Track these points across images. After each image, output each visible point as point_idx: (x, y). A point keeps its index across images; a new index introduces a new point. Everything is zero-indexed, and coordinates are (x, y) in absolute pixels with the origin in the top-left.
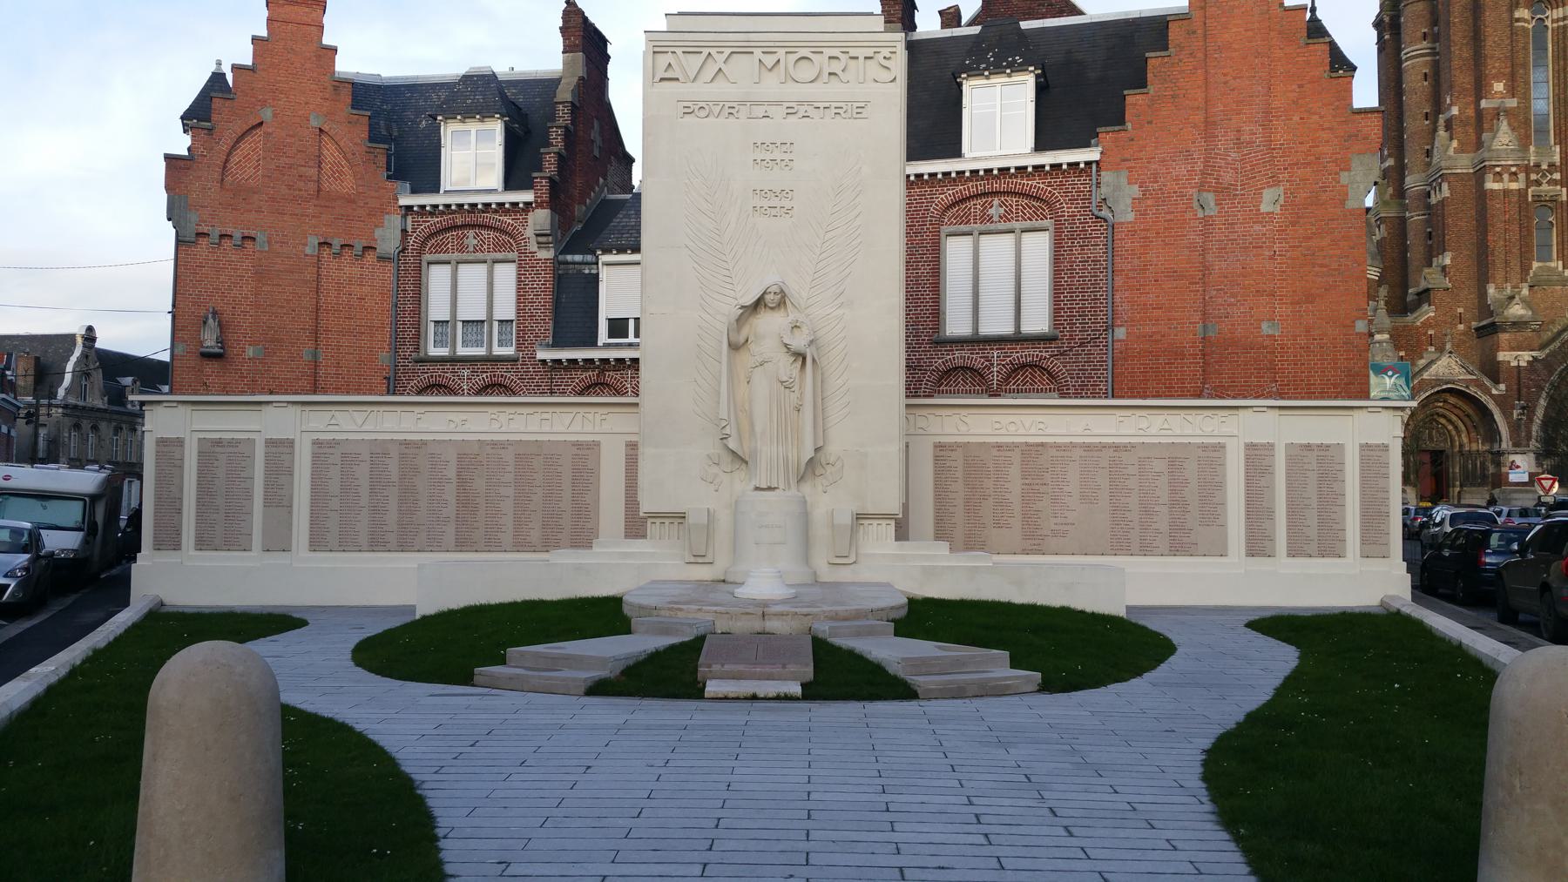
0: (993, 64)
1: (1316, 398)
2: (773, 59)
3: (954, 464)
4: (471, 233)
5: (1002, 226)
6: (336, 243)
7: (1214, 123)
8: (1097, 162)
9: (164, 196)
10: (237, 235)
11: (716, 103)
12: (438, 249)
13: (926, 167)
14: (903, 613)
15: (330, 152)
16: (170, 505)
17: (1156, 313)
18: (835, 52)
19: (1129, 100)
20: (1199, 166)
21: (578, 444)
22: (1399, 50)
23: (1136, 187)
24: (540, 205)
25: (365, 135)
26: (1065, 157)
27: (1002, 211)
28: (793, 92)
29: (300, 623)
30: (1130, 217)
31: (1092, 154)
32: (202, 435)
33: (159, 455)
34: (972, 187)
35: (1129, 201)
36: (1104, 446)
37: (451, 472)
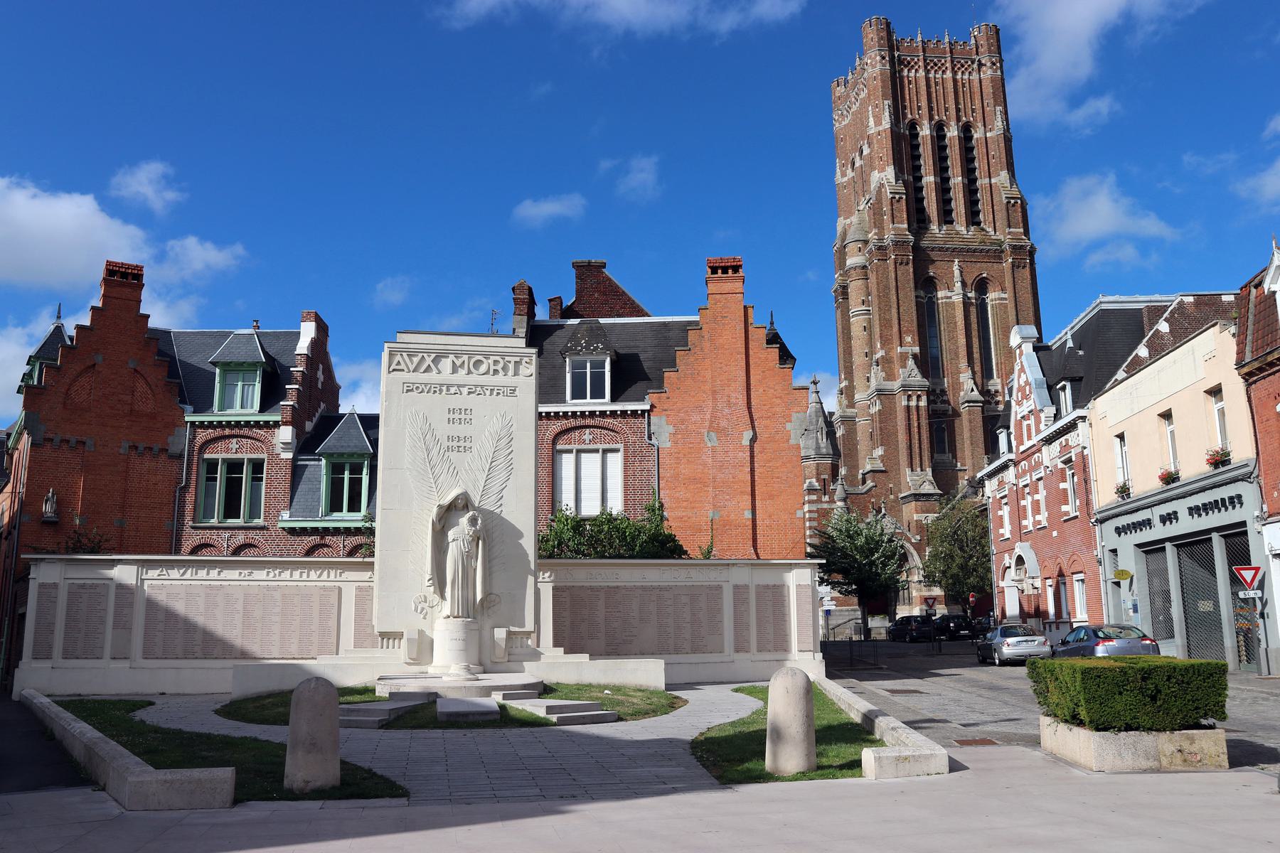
4: (235, 440)
8: (649, 411)
10: (73, 440)
11: (426, 384)
14: (338, 783)
15: (141, 386)
16: (45, 626)
18: (497, 358)
20: (708, 416)
24: (285, 424)
25: (165, 374)
28: (475, 379)
29: (151, 704)
30: (669, 445)
33: (40, 594)
34: (572, 423)
36: (654, 588)
37: (239, 606)
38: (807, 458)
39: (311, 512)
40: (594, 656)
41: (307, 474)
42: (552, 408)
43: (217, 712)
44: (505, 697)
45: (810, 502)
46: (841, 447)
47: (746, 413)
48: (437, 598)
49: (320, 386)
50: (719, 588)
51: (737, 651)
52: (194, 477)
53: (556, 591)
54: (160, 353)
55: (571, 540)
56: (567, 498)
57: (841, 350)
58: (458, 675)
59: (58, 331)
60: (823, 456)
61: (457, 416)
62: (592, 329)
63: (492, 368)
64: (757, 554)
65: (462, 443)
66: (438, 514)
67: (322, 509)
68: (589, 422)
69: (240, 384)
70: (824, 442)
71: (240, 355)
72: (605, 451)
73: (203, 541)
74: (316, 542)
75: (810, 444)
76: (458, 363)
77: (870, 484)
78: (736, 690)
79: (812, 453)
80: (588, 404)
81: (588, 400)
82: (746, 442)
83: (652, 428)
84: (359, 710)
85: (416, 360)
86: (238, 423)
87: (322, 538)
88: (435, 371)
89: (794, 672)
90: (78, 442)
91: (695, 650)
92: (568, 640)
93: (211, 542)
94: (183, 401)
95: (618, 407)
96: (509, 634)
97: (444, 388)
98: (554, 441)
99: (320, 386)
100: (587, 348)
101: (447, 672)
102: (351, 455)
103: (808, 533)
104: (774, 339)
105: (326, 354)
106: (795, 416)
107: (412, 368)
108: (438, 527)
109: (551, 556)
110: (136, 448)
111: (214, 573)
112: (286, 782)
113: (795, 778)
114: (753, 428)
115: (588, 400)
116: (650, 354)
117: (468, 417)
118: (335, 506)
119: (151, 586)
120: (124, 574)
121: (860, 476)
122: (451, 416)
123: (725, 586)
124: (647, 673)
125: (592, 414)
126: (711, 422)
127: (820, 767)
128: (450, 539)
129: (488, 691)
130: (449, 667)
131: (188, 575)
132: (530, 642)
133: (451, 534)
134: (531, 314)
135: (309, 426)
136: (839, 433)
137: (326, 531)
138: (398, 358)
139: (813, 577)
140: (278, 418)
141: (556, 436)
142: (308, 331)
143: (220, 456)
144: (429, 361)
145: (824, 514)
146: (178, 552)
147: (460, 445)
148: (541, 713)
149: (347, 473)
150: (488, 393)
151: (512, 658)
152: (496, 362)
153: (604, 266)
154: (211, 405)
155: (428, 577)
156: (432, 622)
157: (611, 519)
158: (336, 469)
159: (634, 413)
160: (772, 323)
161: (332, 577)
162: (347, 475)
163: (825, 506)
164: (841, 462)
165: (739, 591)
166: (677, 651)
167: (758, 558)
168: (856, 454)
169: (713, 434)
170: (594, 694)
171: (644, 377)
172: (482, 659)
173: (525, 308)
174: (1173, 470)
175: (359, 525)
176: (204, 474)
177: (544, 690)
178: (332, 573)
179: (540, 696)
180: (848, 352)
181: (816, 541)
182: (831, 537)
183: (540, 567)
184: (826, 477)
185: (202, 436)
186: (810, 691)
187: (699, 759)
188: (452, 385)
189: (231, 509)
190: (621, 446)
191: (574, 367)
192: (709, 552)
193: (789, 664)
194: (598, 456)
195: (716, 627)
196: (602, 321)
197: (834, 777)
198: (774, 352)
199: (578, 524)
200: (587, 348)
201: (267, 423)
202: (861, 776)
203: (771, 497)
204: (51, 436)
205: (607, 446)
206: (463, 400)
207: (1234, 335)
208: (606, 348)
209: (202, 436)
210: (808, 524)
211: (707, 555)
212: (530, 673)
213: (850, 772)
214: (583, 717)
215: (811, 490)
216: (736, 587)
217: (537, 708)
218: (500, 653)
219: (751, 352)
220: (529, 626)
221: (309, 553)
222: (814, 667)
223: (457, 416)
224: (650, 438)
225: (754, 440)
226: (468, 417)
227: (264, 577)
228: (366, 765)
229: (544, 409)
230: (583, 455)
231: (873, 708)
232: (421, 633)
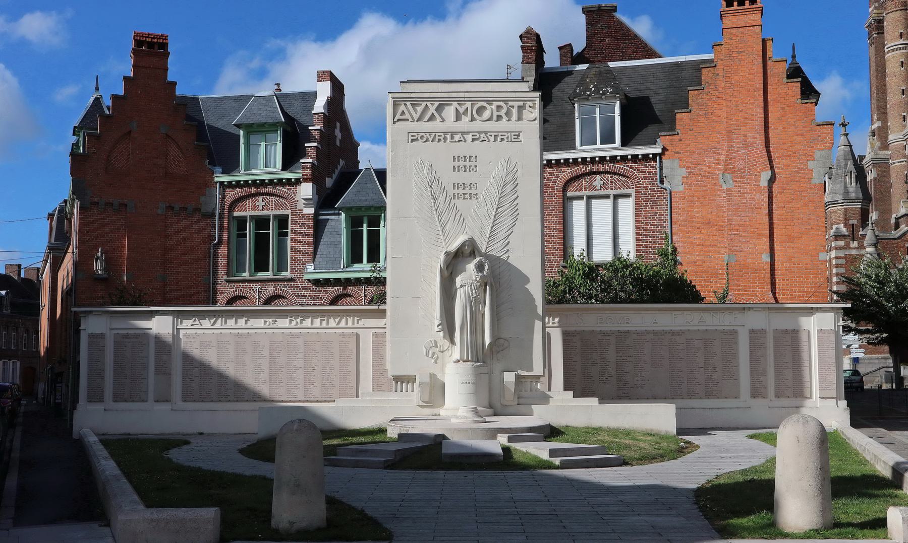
0: (594, 92)
2: (464, 108)
4: (260, 198)
5: (602, 192)
6: (177, 207)
8: (660, 155)
9: (70, 179)
11: (430, 133)
13: (553, 156)
14: (323, 524)
16: (97, 374)
17: (698, 248)
19: (678, 116)
22: (884, 45)
23: (684, 170)
24: (306, 180)
26: (641, 151)
28: (478, 125)
29: (187, 442)
30: (681, 188)
32: (116, 332)
33: (90, 344)
34: (582, 169)
35: (680, 178)
37: (266, 353)
38: (835, 203)
39: (333, 264)
40: (603, 400)
41: (328, 228)
42: (562, 155)
43: (242, 451)
44: (510, 439)
45: (837, 248)
46: (872, 191)
47: (764, 152)
48: (447, 343)
49: (338, 143)
50: (734, 333)
51: (754, 396)
52: (225, 234)
53: (568, 338)
54: (189, 118)
55: (579, 285)
56: (578, 246)
57: (874, 89)
58: (465, 417)
59: (97, 101)
60: (852, 201)
61: (462, 163)
62: (600, 73)
63: (496, 113)
64: (776, 298)
65: (467, 191)
66: (445, 261)
67: (343, 261)
68: (599, 167)
69: (263, 144)
70: (853, 187)
71: (262, 117)
72: (616, 197)
73: (237, 294)
74: (340, 291)
75: (839, 190)
76: (461, 110)
77: (903, 228)
78: (751, 437)
79: (839, 198)
80: (599, 150)
81: (599, 146)
82: (764, 183)
83: (664, 171)
84: (366, 451)
85: (420, 109)
86: (263, 181)
87: (345, 288)
88: (439, 119)
89: (806, 420)
90: (121, 205)
91: (709, 395)
92: (578, 385)
93: (244, 294)
94: (212, 163)
95: (629, 152)
96: (518, 377)
97: (449, 136)
98: (565, 189)
99: (338, 143)
100: (596, 92)
101: (455, 415)
102: (369, 208)
103: (835, 279)
104: (795, 72)
105: (343, 112)
106: (818, 154)
107: (416, 117)
108: (446, 274)
109: (561, 301)
110: (173, 208)
111: (241, 322)
112: (272, 523)
113: (807, 536)
114: (772, 168)
115: (599, 146)
116: (662, 97)
117: (473, 164)
118: (355, 257)
119: (186, 335)
120: (159, 325)
121: (893, 221)
122: (456, 164)
123: (739, 329)
124: (660, 417)
125: (603, 159)
126: (727, 164)
127: (837, 525)
128: (458, 285)
129: (493, 434)
130: (458, 409)
131: (218, 325)
132: (539, 386)
133: (459, 281)
134: (540, 62)
135: (329, 182)
136: (870, 177)
137: (348, 282)
138: (402, 108)
139: (836, 321)
140: (299, 175)
141: (565, 184)
142: (324, 91)
143: (248, 213)
144: (432, 109)
145: (852, 261)
146: (214, 303)
147: (467, 192)
148: (545, 456)
149: (365, 226)
150: (492, 139)
151: (521, 401)
152: (499, 108)
153: (614, 9)
154: (237, 165)
155: (437, 322)
156: (444, 365)
157: (626, 265)
158: (355, 223)
159: (645, 157)
160: (794, 57)
161: (350, 324)
162: (365, 228)
163: (854, 252)
164: (872, 206)
165: (756, 335)
166: (691, 395)
167: (777, 302)
168: (889, 198)
169: (728, 176)
170: (601, 438)
171: (654, 119)
172: (492, 403)
173: (533, 56)
175: (368, 275)
176: (234, 232)
177: (551, 432)
178: (350, 320)
179: (546, 438)
180: (882, 91)
181: (843, 288)
182: (858, 285)
183: (547, 313)
184: (855, 222)
185: (231, 194)
186: (826, 441)
187: (702, 509)
188: (456, 133)
189: (261, 264)
190: (631, 191)
191: (581, 113)
192: (725, 297)
193: (805, 411)
194: (609, 203)
195: (731, 372)
196: (612, 64)
197: (854, 537)
198: (795, 87)
199: (591, 271)
200: (596, 92)
201: (289, 180)
202: (886, 537)
203: (791, 239)
204: (97, 200)
205: (618, 192)
206: (468, 147)
207: (880, 386)
208: (616, 91)
209: (231, 194)
210: (834, 271)
211: (723, 299)
212: (539, 416)
213: (872, 532)
214: (587, 460)
215: (838, 236)
216: (752, 332)
217: (540, 450)
218: (510, 397)
219: (770, 88)
220: (538, 368)
221: (334, 302)
222: (835, 415)
223: (462, 163)
224: (662, 182)
225: (772, 180)
226: (473, 164)
227: (287, 325)
228: (358, 505)
229: (553, 156)
230: (594, 201)
231: (901, 459)
232: (433, 376)
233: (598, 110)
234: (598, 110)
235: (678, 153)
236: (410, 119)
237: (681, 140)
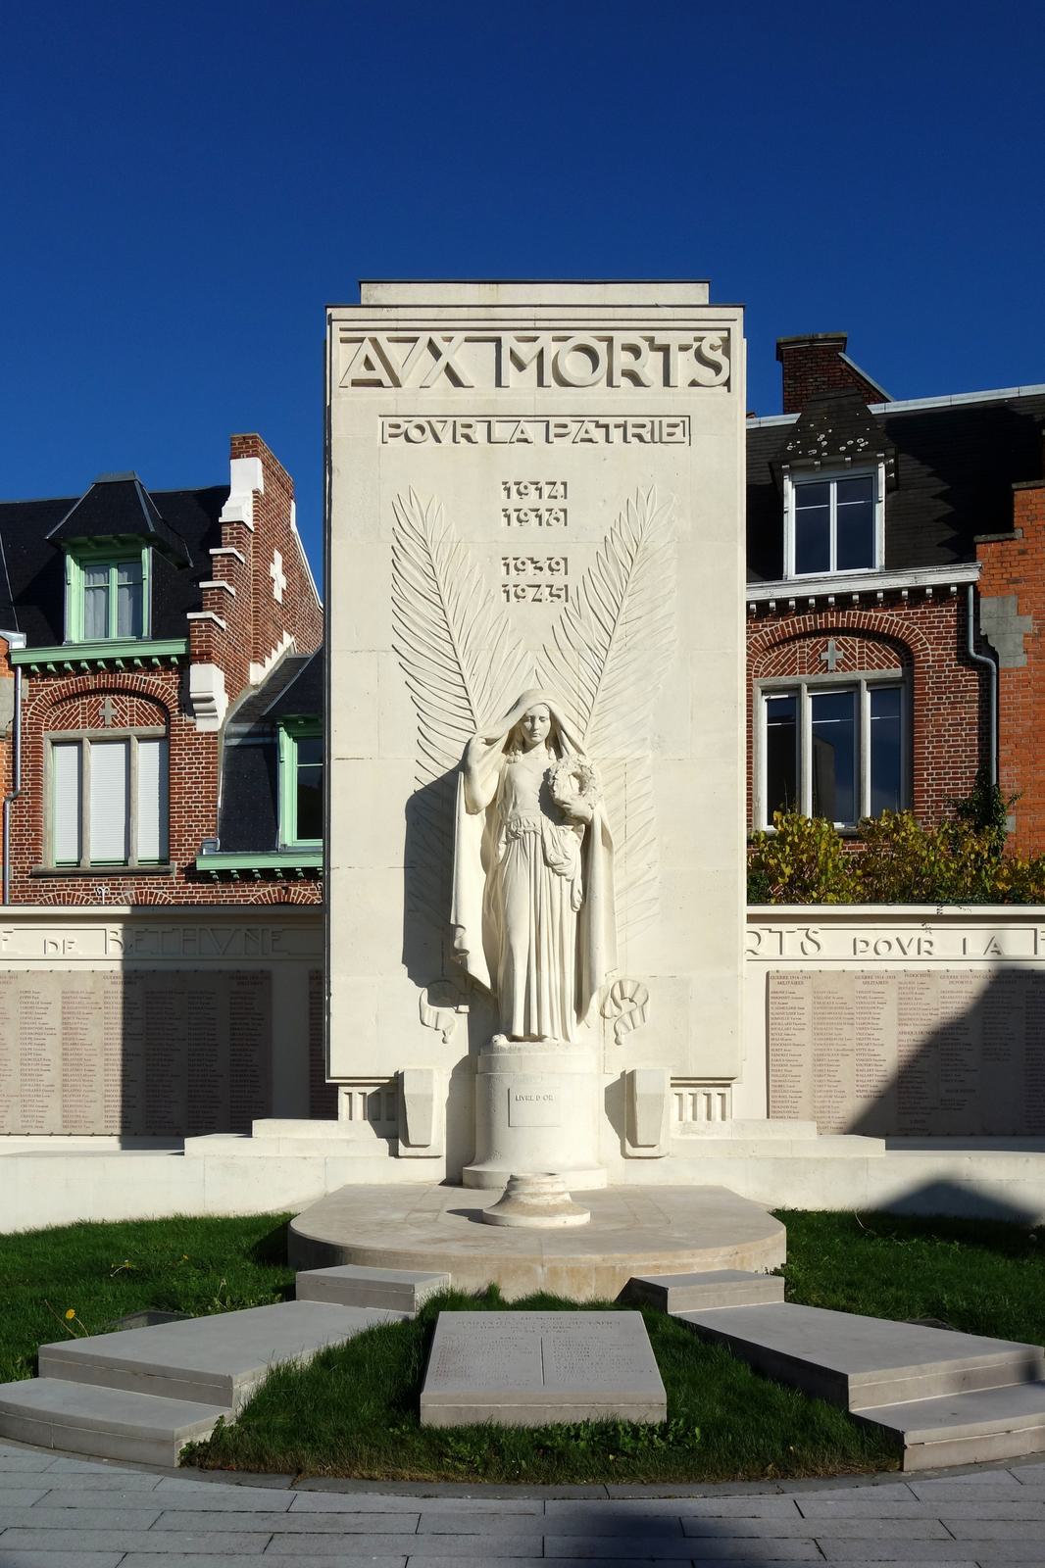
1: (887, 902)
3: (795, 1071)
4: (109, 699)
7: (268, 1424)
12: (64, 722)
19: (1019, 496)
21: (239, 977)
23: (1029, 619)
27: (840, 654)
31: (969, 575)
35: (1019, 639)
37: (54, 1019)
49: (278, 596)
68: (833, 620)
80: (835, 581)
99: (278, 596)
100: (832, 449)
125: (844, 600)
174: (495, 1281)
196: (787, 696)
226: (556, 504)
233: (833, 488)
234: (833, 488)
235: (1016, 581)
236: (386, 380)
237: (1023, 552)
